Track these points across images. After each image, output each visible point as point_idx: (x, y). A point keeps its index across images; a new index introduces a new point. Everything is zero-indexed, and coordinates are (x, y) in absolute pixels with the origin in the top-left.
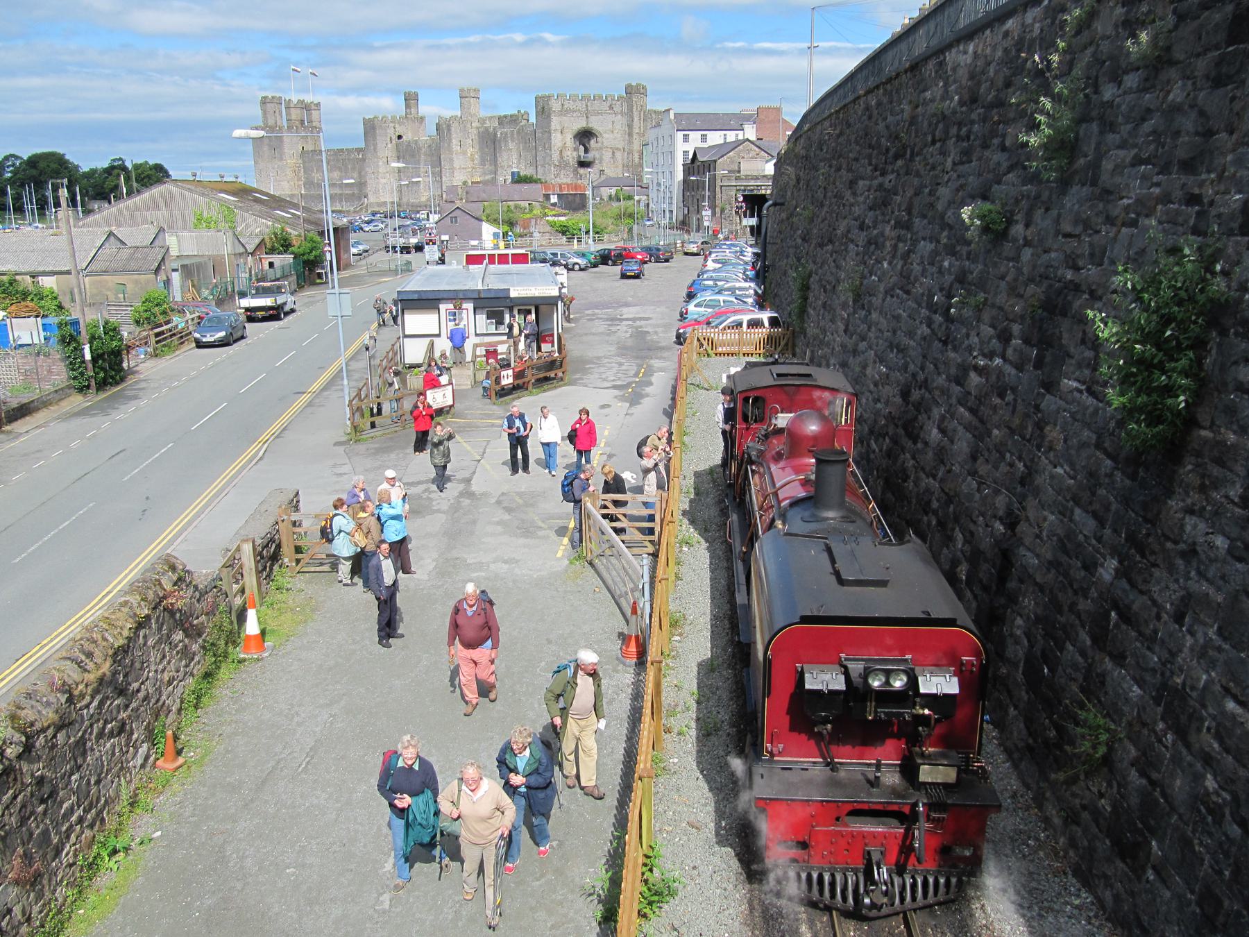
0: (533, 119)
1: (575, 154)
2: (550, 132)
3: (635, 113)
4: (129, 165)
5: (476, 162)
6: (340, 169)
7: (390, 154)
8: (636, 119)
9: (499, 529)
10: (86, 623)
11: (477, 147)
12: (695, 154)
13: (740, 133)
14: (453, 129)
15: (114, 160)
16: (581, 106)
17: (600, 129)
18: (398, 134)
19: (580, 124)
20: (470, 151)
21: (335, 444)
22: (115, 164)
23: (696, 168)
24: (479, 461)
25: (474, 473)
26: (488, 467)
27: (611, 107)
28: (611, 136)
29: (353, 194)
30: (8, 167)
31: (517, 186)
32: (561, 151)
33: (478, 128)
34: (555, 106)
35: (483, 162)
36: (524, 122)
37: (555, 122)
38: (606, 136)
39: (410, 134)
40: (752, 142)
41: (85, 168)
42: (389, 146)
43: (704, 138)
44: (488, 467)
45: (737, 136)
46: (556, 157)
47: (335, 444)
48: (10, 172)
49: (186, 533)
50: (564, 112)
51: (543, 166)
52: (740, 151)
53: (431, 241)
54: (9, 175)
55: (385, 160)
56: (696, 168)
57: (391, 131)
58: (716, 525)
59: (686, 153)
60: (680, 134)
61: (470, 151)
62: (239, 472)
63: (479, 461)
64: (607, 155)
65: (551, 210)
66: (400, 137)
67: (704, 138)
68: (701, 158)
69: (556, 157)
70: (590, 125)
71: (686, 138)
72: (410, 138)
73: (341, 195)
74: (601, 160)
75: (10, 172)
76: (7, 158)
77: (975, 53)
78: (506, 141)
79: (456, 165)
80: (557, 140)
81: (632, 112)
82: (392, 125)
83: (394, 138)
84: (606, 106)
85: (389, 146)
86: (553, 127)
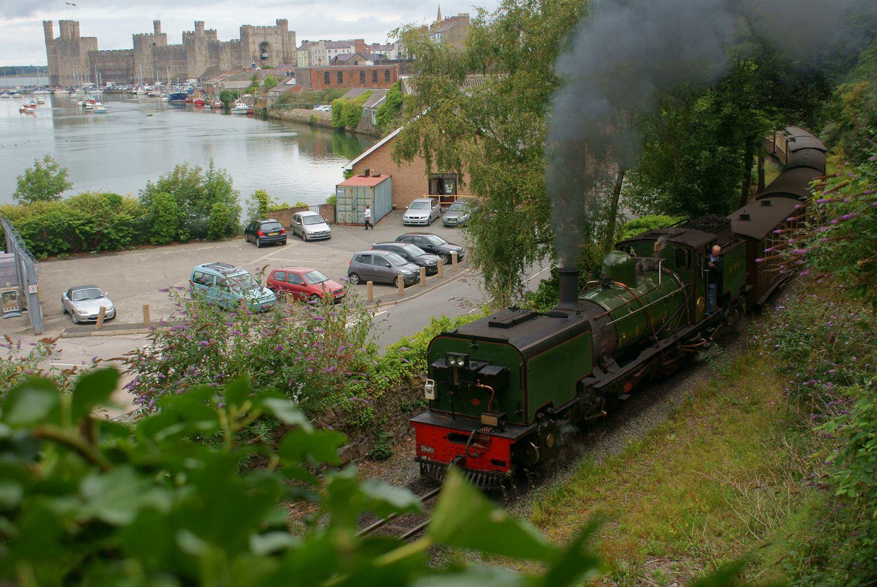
2: (248, 44)
5: (208, 58)
6: (114, 61)
8: (285, 36)
10: (415, 238)
11: (208, 51)
16: (262, 31)
19: (262, 40)
29: (123, 74)
31: (264, 70)
32: (254, 53)
33: (208, 41)
34: (251, 32)
35: (211, 58)
37: (251, 39)
38: (274, 45)
39: (159, 43)
42: (149, 49)
46: (251, 55)
50: (255, 34)
55: (146, 56)
57: (150, 42)
58: (825, 78)
60: (327, 50)
61: (204, 52)
66: (154, 44)
69: (251, 55)
70: (267, 40)
71: (329, 51)
79: (198, 59)
83: (152, 45)
84: (273, 31)
85: (149, 49)
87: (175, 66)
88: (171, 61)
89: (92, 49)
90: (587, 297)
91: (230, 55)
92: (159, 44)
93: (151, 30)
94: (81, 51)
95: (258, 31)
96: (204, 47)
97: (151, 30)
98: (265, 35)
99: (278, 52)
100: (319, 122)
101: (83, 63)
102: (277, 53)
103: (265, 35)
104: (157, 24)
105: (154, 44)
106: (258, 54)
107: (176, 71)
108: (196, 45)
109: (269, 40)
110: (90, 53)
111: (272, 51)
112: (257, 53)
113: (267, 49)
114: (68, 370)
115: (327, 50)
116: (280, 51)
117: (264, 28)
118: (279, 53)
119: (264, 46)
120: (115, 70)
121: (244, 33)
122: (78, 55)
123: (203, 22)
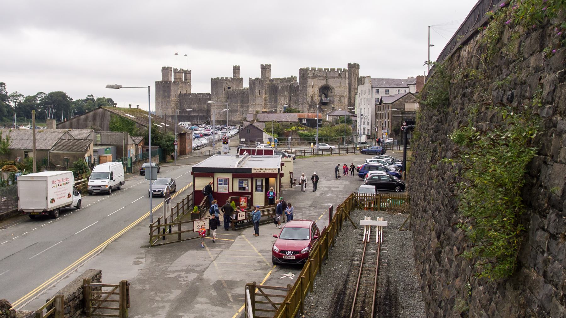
0: (298, 81)
1: (319, 98)
2: (306, 87)
3: (353, 78)
4: (95, 98)
7: (223, 97)
8: (353, 81)
9: (367, 231)
12: (381, 99)
13: (407, 89)
14: (256, 84)
15: (88, 96)
17: (333, 86)
18: (228, 86)
19: (322, 83)
20: (264, 96)
21: (142, 247)
22: (89, 98)
23: (382, 107)
24: (212, 261)
25: (207, 268)
26: (216, 265)
27: (339, 75)
28: (339, 89)
30: (39, 98)
32: (312, 97)
33: (269, 84)
34: (310, 74)
35: (271, 101)
36: (294, 81)
37: (310, 82)
40: (412, 94)
41: (74, 100)
42: (224, 92)
43: (387, 92)
44: (216, 265)
45: (405, 90)
47: (142, 247)
48: (40, 101)
49: (46, 289)
50: (314, 77)
51: (302, 104)
52: (406, 98)
53: (225, 141)
54: (39, 102)
55: (221, 99)
56: (382, 107)
57: (225, 85)
59: (377, 99)
62: (88, 258)
63: (212, 261)
64: (336, 99)
65: (302, 127)
66: (229, 88)
67: (387, 92)
68: (384, 102)
69: (309, 99)
72: (234, 89)
73: (197, 116)
74: (333, 102)
75: (40, 101)
76: (38, 94)
77: (468, 51)
78: (283, 91)
80: (310, 91)
81: (351, 77)
82: (226, 82)
84: (337, 75)
86: (308, 85)
87: (242, 109)
88: (239, 105)
89: (184, 92)
90: (542, 132)
91: (288, 99)
92: (234, 88)
93: (230, 75)
94: (172, 93)
95: (319, 73)
96: (264, 91)
97: (230, 75)
98: (326, 78)
99: (341, 97)
100: (26, 211)
101: (172, 104)
102: (340, 98)
103: (326, 78)
104: (236, 69)
105: (229, 88)
106: (317, 99)
107: (243, 114)
108: (257, 88)
109: (332, 83)
110: (181, 95)
111: (334, 96)
112: (316, 98)
113: (329, 94)
114: (128, 307)
115: (374, 89)
116: (343, 96)
117: (326, 70)
118: (343, 99)
119: (325, 90)
120: (198, 112)
121: (303, 74)
122: (169, 97)
123: (270, 66)
